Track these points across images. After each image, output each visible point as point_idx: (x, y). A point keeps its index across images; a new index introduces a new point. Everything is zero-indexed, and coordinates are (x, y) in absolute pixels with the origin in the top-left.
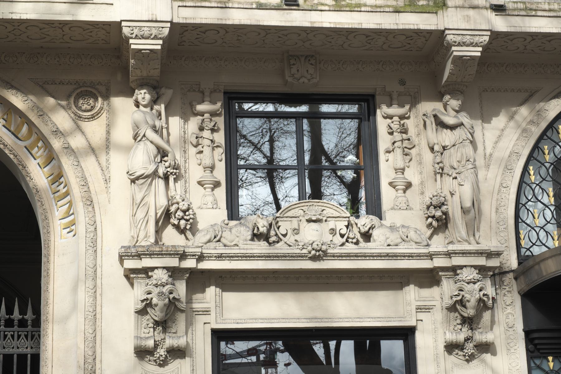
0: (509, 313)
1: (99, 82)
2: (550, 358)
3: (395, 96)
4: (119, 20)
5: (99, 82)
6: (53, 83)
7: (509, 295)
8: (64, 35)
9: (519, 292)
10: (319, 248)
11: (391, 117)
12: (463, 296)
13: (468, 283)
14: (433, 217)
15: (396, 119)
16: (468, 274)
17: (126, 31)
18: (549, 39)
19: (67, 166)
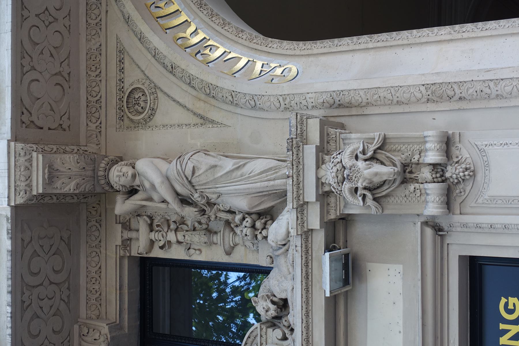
4: (9, 209)
11: (152, 243)
12: (365, 188)
15: (152, 236)
16: (329, 173)
17: (20, 201)
18: (27, 46)
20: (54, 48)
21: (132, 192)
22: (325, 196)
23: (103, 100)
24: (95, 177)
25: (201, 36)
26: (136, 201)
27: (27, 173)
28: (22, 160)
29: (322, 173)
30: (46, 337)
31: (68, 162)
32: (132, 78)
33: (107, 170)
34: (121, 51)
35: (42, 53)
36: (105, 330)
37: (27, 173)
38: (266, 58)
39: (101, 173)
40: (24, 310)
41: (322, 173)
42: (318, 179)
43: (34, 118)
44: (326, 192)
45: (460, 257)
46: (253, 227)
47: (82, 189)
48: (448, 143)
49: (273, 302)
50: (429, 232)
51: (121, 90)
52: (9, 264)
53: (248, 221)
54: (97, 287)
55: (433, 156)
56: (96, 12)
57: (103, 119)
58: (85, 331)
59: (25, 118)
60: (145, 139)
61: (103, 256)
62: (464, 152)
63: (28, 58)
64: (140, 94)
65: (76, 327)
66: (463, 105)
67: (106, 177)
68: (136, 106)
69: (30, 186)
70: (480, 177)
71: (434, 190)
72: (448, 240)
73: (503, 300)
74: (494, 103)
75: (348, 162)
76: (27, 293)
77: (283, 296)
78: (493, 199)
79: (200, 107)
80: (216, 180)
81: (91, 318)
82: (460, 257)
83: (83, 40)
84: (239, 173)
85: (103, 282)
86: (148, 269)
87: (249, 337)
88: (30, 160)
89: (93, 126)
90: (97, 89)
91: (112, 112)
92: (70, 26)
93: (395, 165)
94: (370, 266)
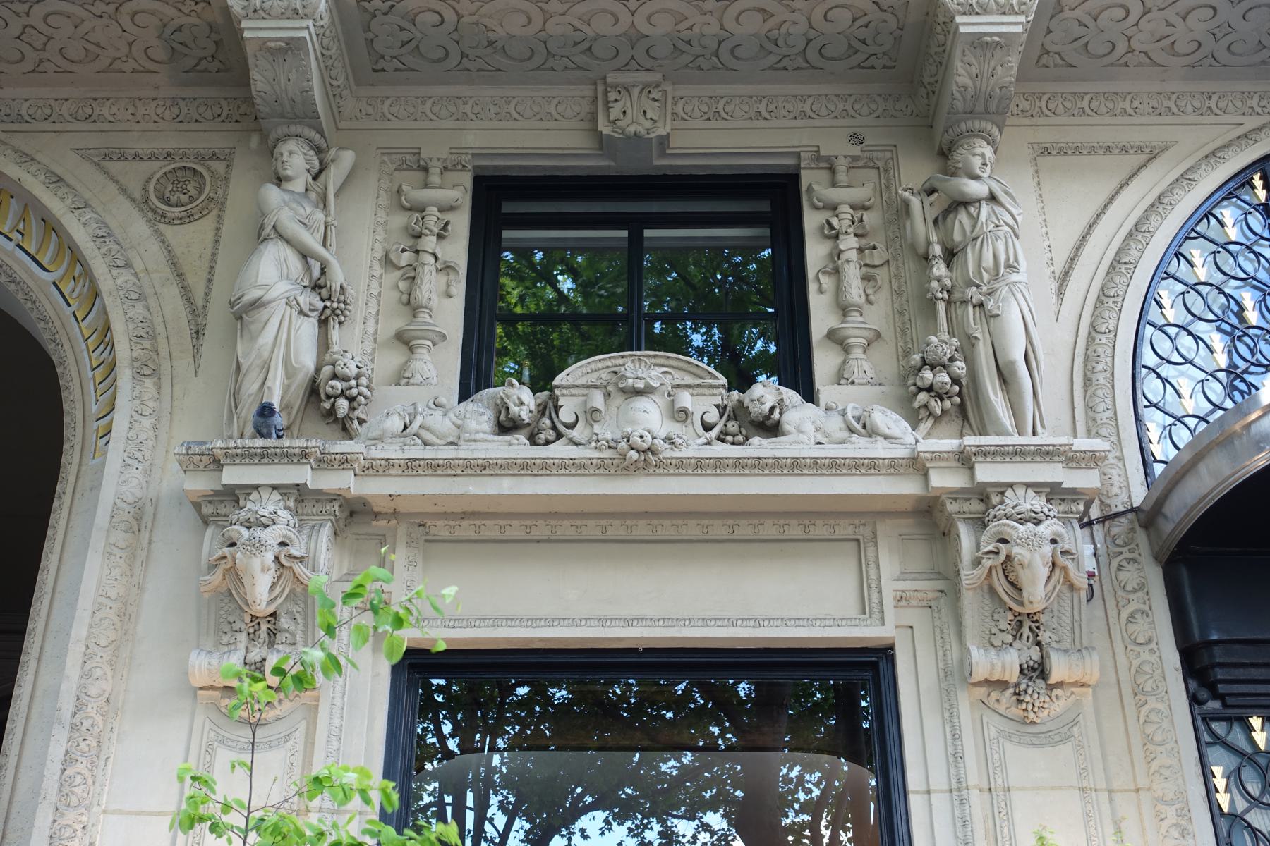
0: (1137, 611)
1: (214, 154)
2: (1256, 722)
3: (841, 166)
5: (214, 154)
6: (122, 157)
7: (1131, 567)
8: (130, 44)
9: (1156, 559)
10: (645, 446)
13: (1022, 521)
14: (930, 389)
19: (111, 299)
20: (417, 46)
29: (1020, 491)
30: (18, 38)
31: (1008, 69)
35: (402, 29)
42: (256, 487)
43: (380, 18)
44: (988, 498)
49: (772, 409)
58: (656, 94)
77: (786, 427)
87: (689, 363)
90: (1060, 109)
92: (383, 70)
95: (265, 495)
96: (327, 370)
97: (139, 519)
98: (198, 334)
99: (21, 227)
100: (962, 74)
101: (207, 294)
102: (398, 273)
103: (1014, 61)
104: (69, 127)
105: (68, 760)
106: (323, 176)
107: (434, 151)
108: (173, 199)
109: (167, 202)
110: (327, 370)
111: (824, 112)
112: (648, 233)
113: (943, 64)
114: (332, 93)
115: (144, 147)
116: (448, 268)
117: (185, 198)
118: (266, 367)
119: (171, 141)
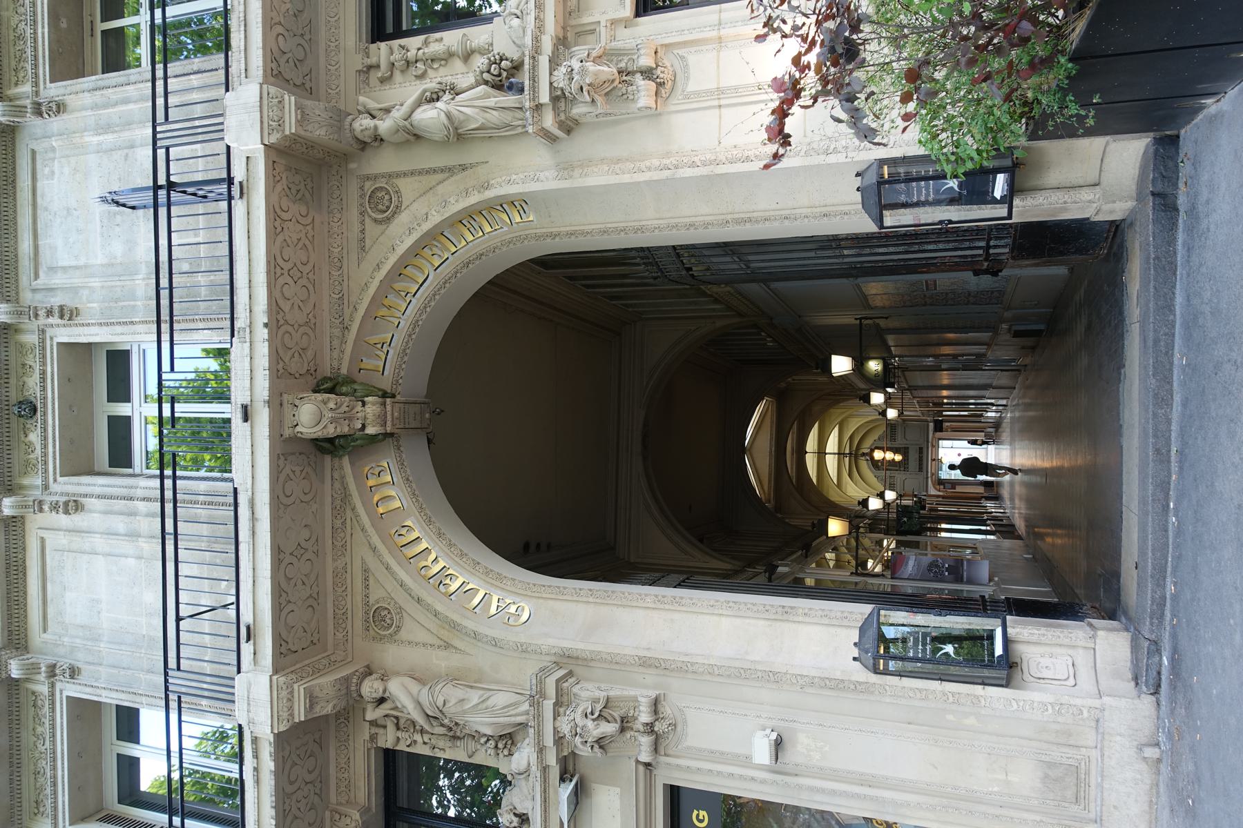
6: (363, 240)
15: (399, 734)
21: (382, 701)
22: (559, 740)
23: (349, 612)
24: (348, 693)
25: (441, 564)
26: (385, 709)
27: (289, 704)
28: (284, 693)
29: (558, 724)
32: (376, 594)
33: (359, 685)
34: (366, 571)
36: (357, 816)
37: (289, 704)
38: (501, 594)
39: (353, 688)
40: (285, 817)
41: (558, 724)
43: (287, 318)
45: (665, 785)
46: (496, 747)
47: (338, 708)
48: (656, 704)
50: (641, 768)
51: (367, 604)
52: (273, 783)
53: (492, 743)
54: (346, 775)
55: (645, 717)
56: (342, 535)
57: (349, 627)
59: (283, 650)
60: (391, 655)
61: (351, 748)
62: (666, 710)
63: (284, 595)
64: (386, 612)
65: (327, 814)
66: (667, 672)
67: (358, 691)
68: (382, 621)
69: (292, 715)
70: (679, 728)
71: (646, 741)
72: (655, 772)
73: (696, 812)
74: (690, 676)
75: (580, 721)
76: (288, 801)
78: (688, 748)
79: (445, 634)
80: (465, 712)
81: (341, 804)
82: (665, 785)
83: (329, 559)
84: (484, 706)
85: (352, 771)
86: (390, 757)
88: (292, 693)
89: (340, 636)
91: (359, 624)
93: (616, 721)
94: (594, 786)
95: (554, 79)
96: (486, 76)
97: (566, 168)
98: (464, 168)
99: (403, 294)
100: (319, 132)
101: (442, 171)
102: (429, 71)
103: (309, 103)
104: (346, 271)
105: (693, 165)
106: (374, 113)
107: (358, 62)
108: (387, 204)
109: (388, 208)
110: (486, 76)
111: (338, 193)
112: (404, 28)
113: (311, 145)
114: (332, 665)
115: (356, 228)
116: (426, 43)
117: (387, 197)
118: (485, 109)
119: (354, 213)
